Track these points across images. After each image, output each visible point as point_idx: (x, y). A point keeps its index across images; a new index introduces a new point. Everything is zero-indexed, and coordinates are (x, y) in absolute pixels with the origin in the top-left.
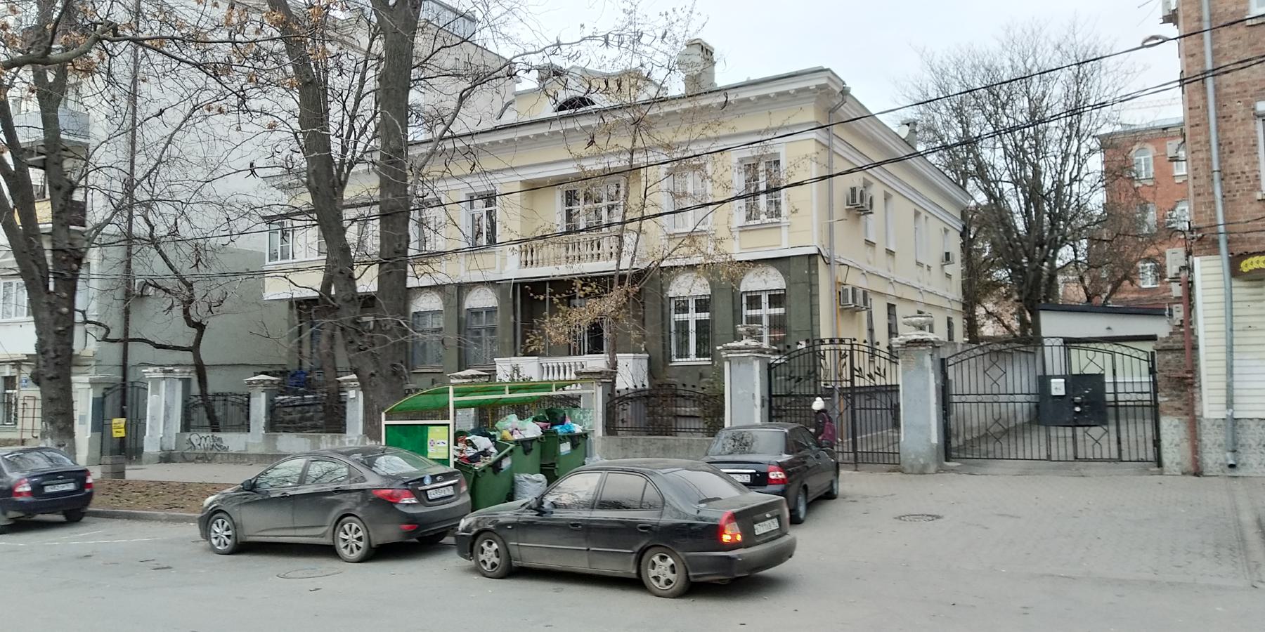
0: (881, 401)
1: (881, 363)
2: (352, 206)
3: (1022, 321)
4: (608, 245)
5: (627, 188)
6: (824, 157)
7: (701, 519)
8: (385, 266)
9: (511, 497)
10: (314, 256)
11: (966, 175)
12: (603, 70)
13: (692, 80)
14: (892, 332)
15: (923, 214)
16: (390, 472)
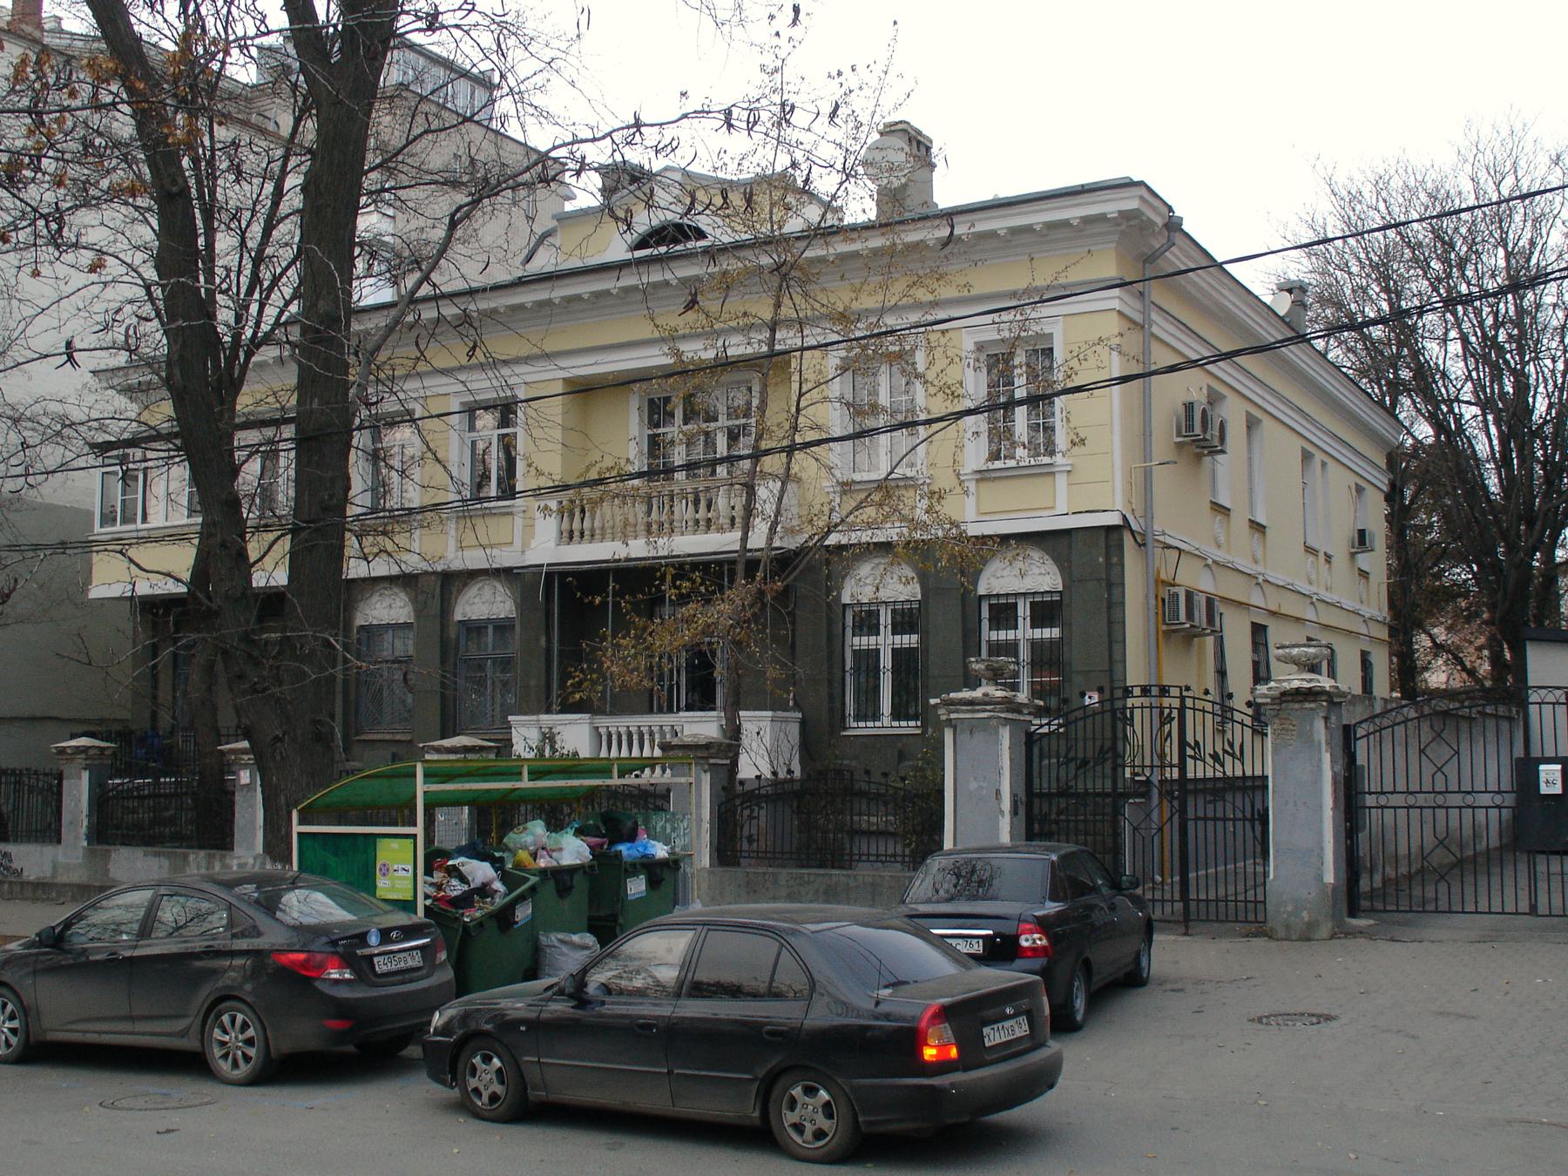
0: (1235, 805)
1: (1240, 734)
2: (247, 425)
3: (1496, 659)
4: (726, 502)
5: (764, 386)
6: (1133, 341)
7: (887, 1017)
8: (304, 535)
9: (532, 974)
10: (180, 518)
11: (1396, 388)
12: (721, 175)
13: (890, 198)
14: (1260, 674)
15: (1319, 457)
16: (307, 921)
